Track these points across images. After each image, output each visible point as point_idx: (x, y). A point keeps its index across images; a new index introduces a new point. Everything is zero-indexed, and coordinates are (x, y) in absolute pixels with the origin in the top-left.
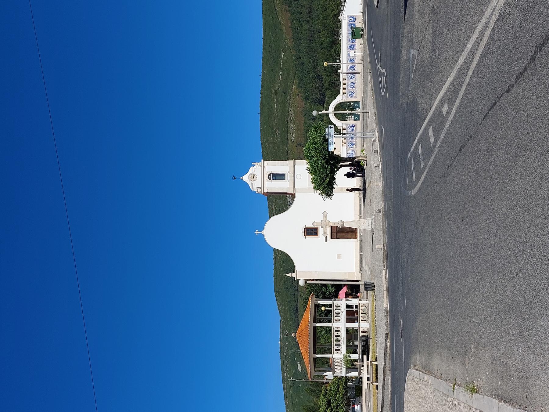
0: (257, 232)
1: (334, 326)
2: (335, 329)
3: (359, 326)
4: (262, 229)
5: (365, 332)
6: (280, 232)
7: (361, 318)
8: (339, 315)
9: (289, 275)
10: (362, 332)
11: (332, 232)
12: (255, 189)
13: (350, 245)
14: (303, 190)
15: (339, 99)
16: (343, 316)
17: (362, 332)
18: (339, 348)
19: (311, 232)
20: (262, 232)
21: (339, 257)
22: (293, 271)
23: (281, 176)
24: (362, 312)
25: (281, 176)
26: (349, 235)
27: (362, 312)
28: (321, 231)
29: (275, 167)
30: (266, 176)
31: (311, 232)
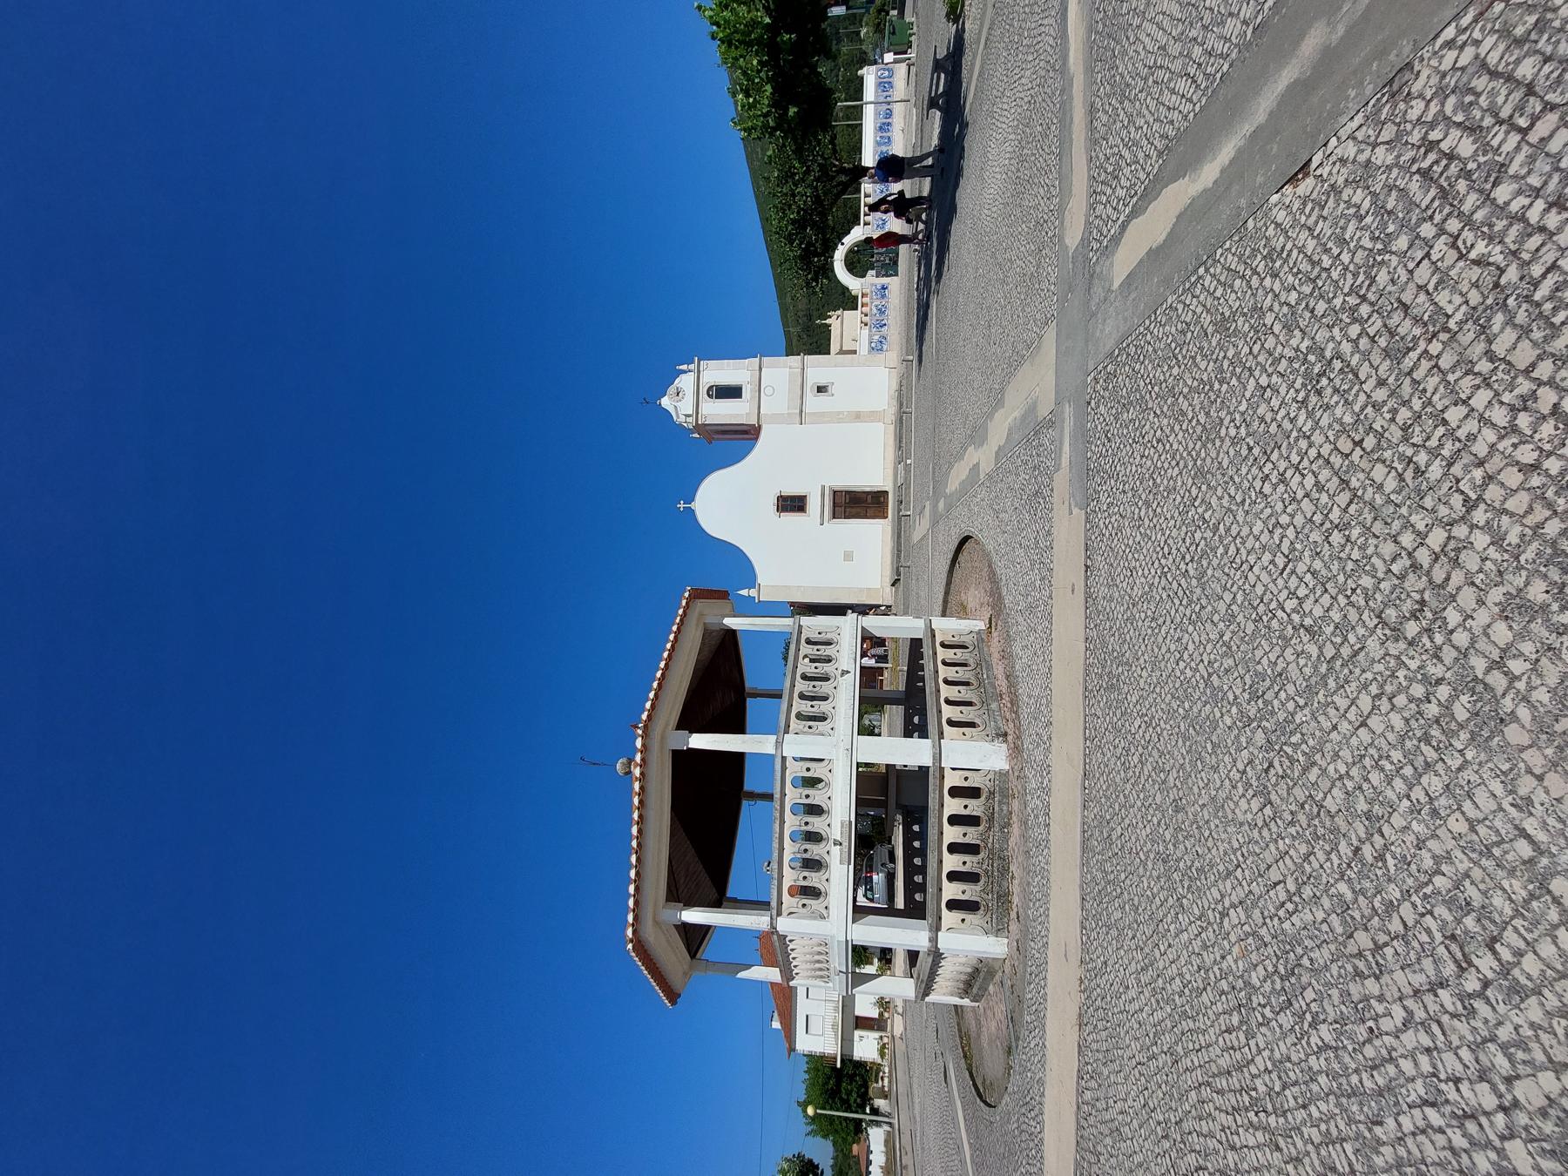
0: (682, 506)
1: (789, 751)
2: (795, 770)
3: (938, 756)
4: (690, 498)
5: (974, 793)
6: (726, 505)
7: (948, 712)
8: (824, 688)
9: (744, 592)
10: (956, 792)
11: (835, 505)
12: (682, 419)
13: (873, 534)
14: (778, 419)
15: (857, 234)
16: (844, 697)
17: (956, 792)
18: (814, 879)
19: (792, 504)
20: (692, 506)
21: (848, 556)
22: (751, 581)
23: (733, 392)
24: (951, 673)
25: (733, 392)
26: (870, 512)
27: (951, 673)
28: (813, 504)
29: (720, 372)
30: (703, 391)
31: (792, 504)
